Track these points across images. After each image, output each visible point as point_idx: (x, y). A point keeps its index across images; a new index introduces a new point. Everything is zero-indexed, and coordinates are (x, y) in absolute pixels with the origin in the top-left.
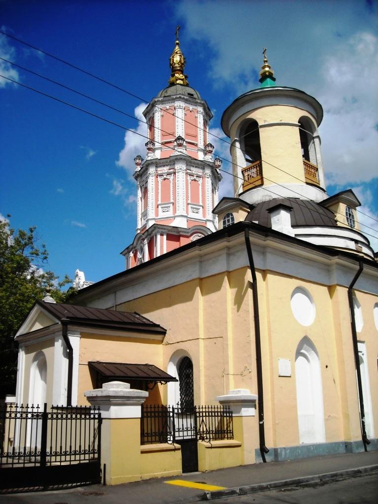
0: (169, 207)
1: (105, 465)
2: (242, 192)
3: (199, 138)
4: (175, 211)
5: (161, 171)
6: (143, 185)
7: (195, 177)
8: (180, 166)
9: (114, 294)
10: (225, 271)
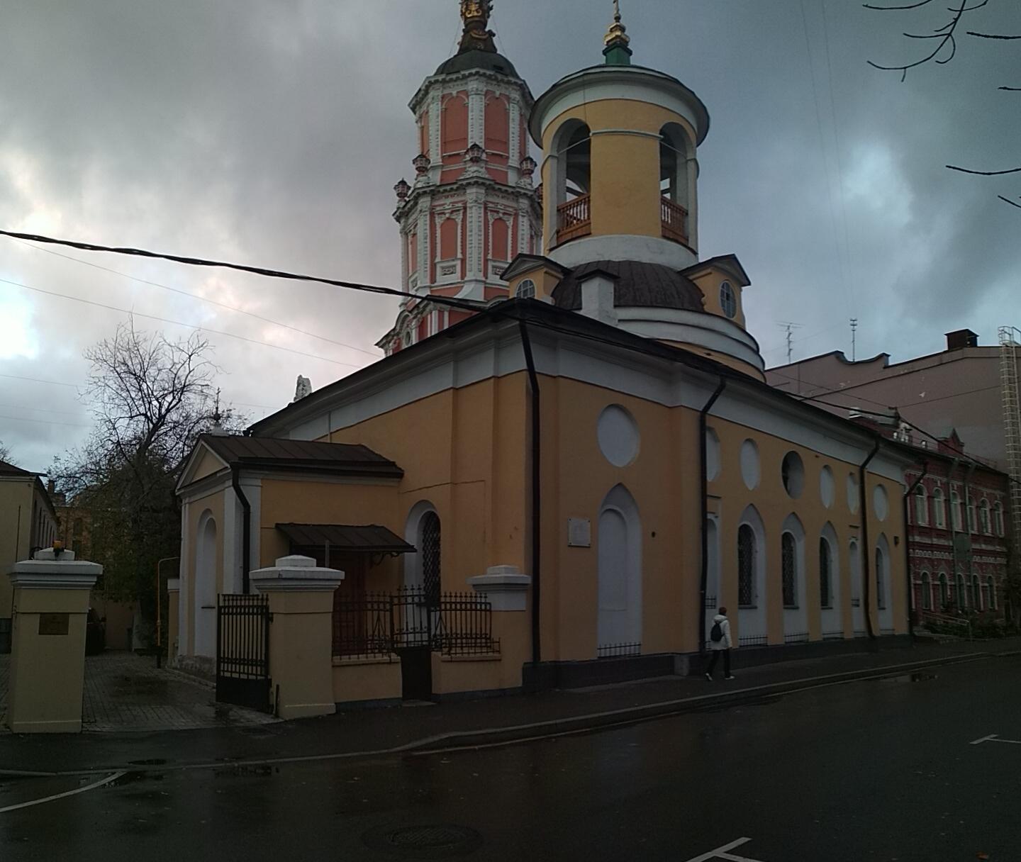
0: (455, 266)
1: (278, 686)
2: (555, 245)
3: (511, 147)
4: (463, 275)
5: (439, 205)
6: (410, 231)
7: (501, 215)
8: (472, 194)
9: (327, 416)
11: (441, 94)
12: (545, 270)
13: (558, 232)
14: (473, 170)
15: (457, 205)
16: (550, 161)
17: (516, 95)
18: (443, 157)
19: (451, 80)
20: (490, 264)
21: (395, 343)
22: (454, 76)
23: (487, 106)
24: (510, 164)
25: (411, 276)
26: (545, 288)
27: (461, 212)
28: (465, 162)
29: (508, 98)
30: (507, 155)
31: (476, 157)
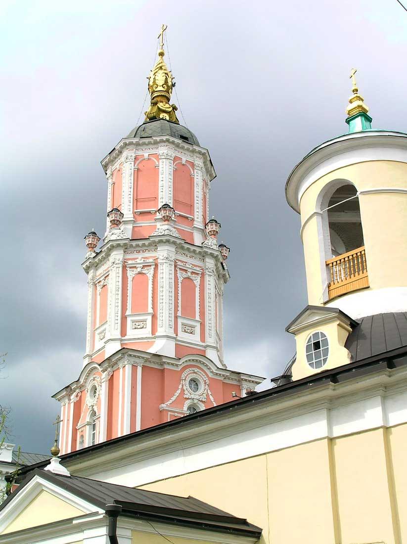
0: (145, 321)
3: (196, 210)
4: (154, 330)
7: (189, 274)
10: (379, 426)
11: (134, 155)
12: (338, 322)
13: (329, 286)
14: (162, 228)
15: (148, 261)
16: (315, 219)
17: (199, 162)
18: (135, 213)
19: (144, 144)
20: (180, 321)
21: (77, 396)
22: (146, 141)
23: (175, 171)
24: (195, 226)
25: (99, 327)
26: (339, 341)
27: (153, 267)
28: (155, 220)
29: (193, 165)
30: (192, 217)
31: (167, 216)
